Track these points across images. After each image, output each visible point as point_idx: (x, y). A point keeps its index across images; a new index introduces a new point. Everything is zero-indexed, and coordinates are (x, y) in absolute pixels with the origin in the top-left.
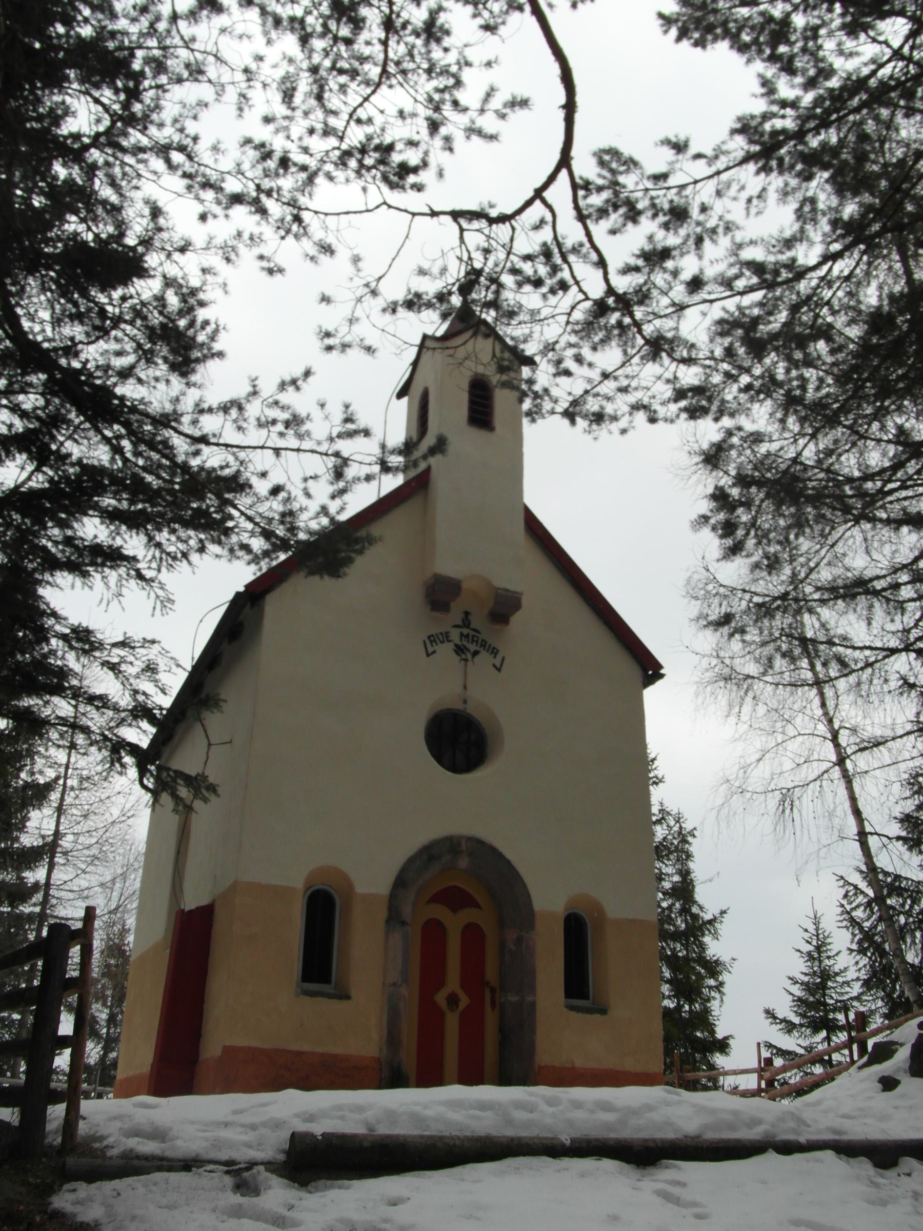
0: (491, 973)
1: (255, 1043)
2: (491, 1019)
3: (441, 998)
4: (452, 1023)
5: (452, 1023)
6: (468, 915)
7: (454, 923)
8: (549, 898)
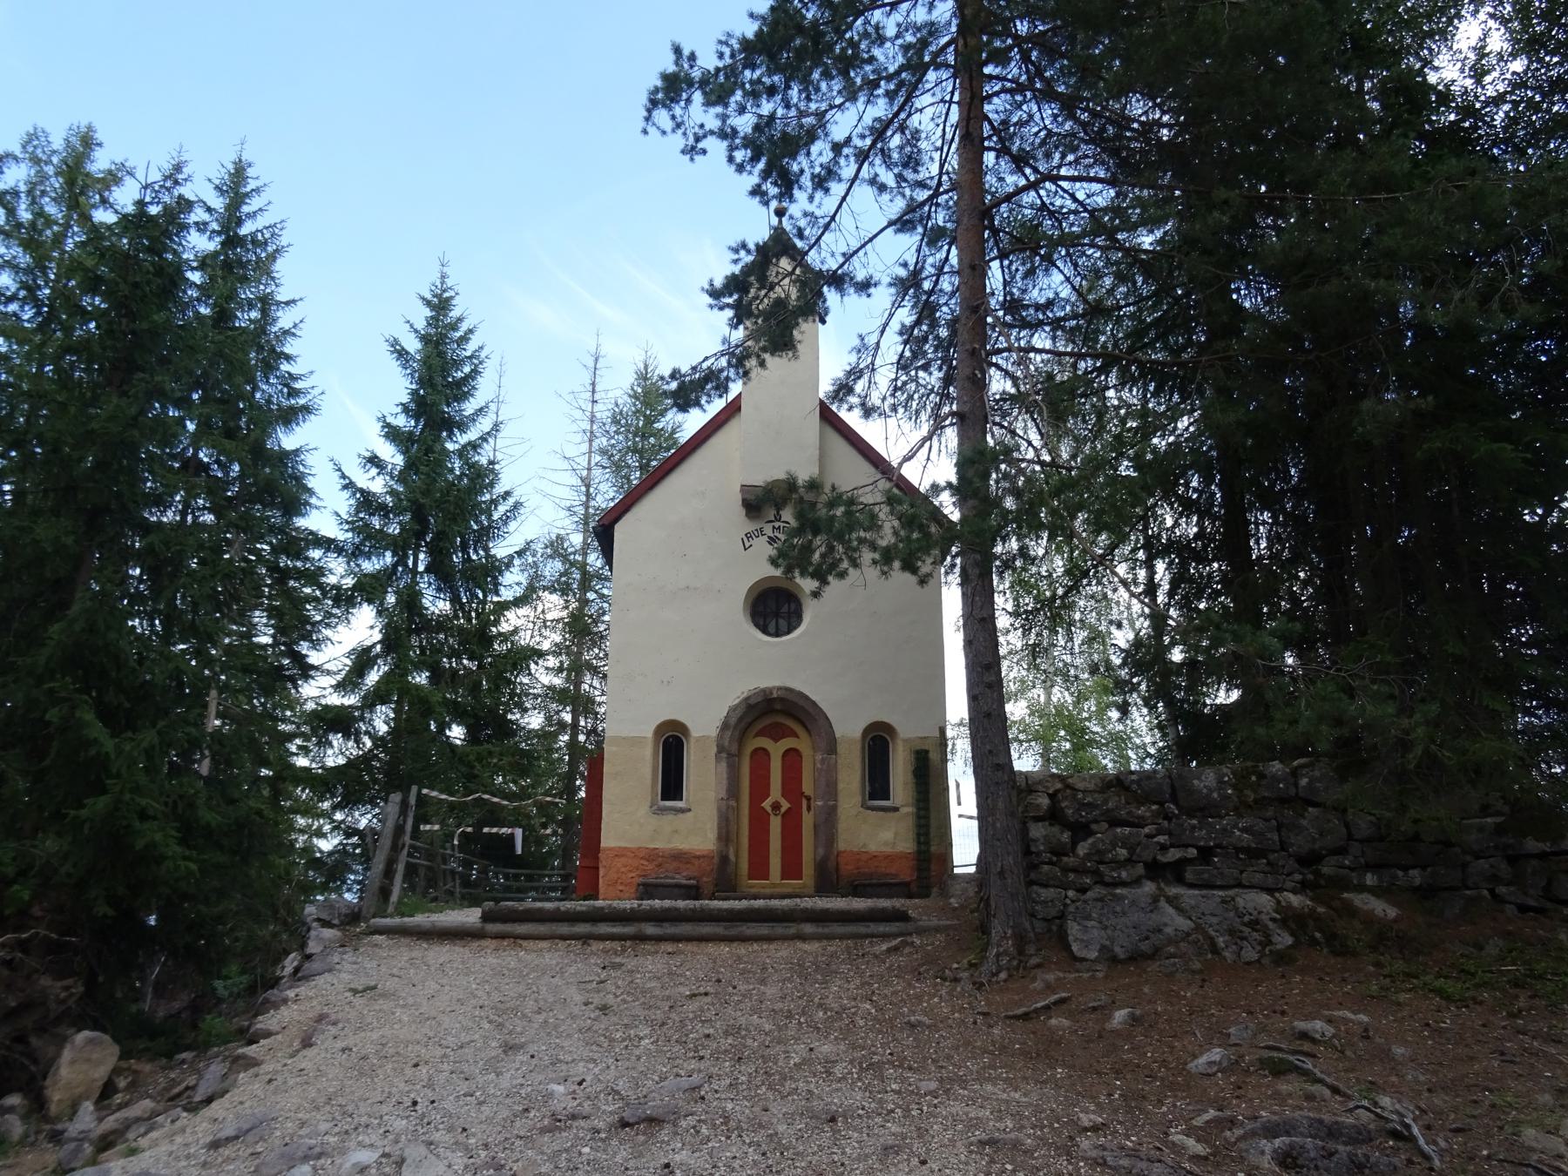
0: (807, 787)
1: (623, 845)
2: (808, 820)
3: (767, 804)
4: (775, 824)
5: (775, 824)
6: (787, 743)
7: (776, 750)
8: (849, 727)
